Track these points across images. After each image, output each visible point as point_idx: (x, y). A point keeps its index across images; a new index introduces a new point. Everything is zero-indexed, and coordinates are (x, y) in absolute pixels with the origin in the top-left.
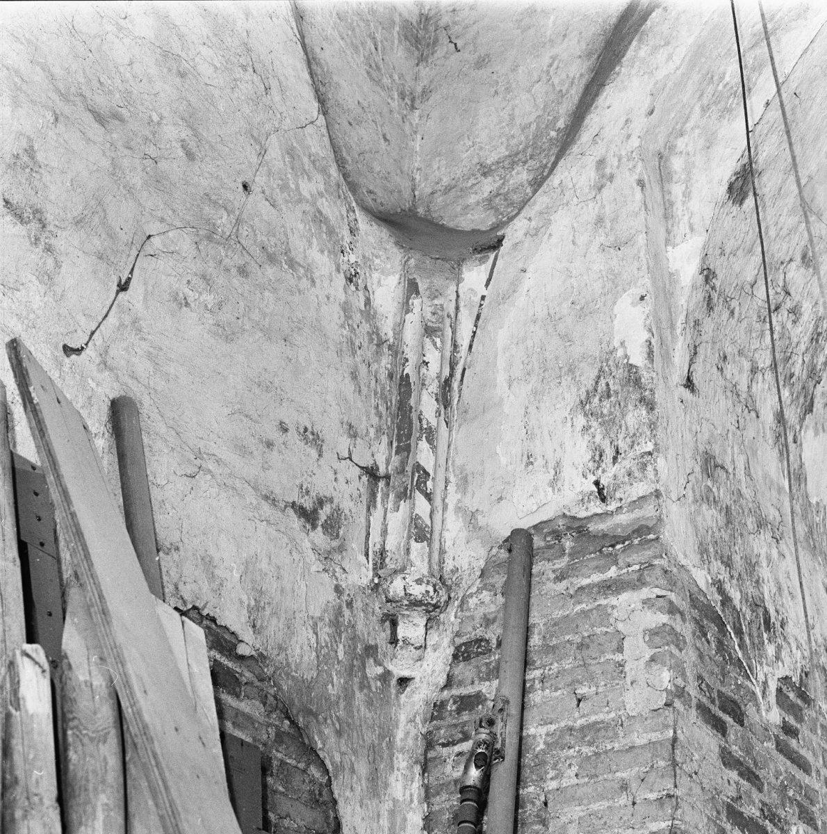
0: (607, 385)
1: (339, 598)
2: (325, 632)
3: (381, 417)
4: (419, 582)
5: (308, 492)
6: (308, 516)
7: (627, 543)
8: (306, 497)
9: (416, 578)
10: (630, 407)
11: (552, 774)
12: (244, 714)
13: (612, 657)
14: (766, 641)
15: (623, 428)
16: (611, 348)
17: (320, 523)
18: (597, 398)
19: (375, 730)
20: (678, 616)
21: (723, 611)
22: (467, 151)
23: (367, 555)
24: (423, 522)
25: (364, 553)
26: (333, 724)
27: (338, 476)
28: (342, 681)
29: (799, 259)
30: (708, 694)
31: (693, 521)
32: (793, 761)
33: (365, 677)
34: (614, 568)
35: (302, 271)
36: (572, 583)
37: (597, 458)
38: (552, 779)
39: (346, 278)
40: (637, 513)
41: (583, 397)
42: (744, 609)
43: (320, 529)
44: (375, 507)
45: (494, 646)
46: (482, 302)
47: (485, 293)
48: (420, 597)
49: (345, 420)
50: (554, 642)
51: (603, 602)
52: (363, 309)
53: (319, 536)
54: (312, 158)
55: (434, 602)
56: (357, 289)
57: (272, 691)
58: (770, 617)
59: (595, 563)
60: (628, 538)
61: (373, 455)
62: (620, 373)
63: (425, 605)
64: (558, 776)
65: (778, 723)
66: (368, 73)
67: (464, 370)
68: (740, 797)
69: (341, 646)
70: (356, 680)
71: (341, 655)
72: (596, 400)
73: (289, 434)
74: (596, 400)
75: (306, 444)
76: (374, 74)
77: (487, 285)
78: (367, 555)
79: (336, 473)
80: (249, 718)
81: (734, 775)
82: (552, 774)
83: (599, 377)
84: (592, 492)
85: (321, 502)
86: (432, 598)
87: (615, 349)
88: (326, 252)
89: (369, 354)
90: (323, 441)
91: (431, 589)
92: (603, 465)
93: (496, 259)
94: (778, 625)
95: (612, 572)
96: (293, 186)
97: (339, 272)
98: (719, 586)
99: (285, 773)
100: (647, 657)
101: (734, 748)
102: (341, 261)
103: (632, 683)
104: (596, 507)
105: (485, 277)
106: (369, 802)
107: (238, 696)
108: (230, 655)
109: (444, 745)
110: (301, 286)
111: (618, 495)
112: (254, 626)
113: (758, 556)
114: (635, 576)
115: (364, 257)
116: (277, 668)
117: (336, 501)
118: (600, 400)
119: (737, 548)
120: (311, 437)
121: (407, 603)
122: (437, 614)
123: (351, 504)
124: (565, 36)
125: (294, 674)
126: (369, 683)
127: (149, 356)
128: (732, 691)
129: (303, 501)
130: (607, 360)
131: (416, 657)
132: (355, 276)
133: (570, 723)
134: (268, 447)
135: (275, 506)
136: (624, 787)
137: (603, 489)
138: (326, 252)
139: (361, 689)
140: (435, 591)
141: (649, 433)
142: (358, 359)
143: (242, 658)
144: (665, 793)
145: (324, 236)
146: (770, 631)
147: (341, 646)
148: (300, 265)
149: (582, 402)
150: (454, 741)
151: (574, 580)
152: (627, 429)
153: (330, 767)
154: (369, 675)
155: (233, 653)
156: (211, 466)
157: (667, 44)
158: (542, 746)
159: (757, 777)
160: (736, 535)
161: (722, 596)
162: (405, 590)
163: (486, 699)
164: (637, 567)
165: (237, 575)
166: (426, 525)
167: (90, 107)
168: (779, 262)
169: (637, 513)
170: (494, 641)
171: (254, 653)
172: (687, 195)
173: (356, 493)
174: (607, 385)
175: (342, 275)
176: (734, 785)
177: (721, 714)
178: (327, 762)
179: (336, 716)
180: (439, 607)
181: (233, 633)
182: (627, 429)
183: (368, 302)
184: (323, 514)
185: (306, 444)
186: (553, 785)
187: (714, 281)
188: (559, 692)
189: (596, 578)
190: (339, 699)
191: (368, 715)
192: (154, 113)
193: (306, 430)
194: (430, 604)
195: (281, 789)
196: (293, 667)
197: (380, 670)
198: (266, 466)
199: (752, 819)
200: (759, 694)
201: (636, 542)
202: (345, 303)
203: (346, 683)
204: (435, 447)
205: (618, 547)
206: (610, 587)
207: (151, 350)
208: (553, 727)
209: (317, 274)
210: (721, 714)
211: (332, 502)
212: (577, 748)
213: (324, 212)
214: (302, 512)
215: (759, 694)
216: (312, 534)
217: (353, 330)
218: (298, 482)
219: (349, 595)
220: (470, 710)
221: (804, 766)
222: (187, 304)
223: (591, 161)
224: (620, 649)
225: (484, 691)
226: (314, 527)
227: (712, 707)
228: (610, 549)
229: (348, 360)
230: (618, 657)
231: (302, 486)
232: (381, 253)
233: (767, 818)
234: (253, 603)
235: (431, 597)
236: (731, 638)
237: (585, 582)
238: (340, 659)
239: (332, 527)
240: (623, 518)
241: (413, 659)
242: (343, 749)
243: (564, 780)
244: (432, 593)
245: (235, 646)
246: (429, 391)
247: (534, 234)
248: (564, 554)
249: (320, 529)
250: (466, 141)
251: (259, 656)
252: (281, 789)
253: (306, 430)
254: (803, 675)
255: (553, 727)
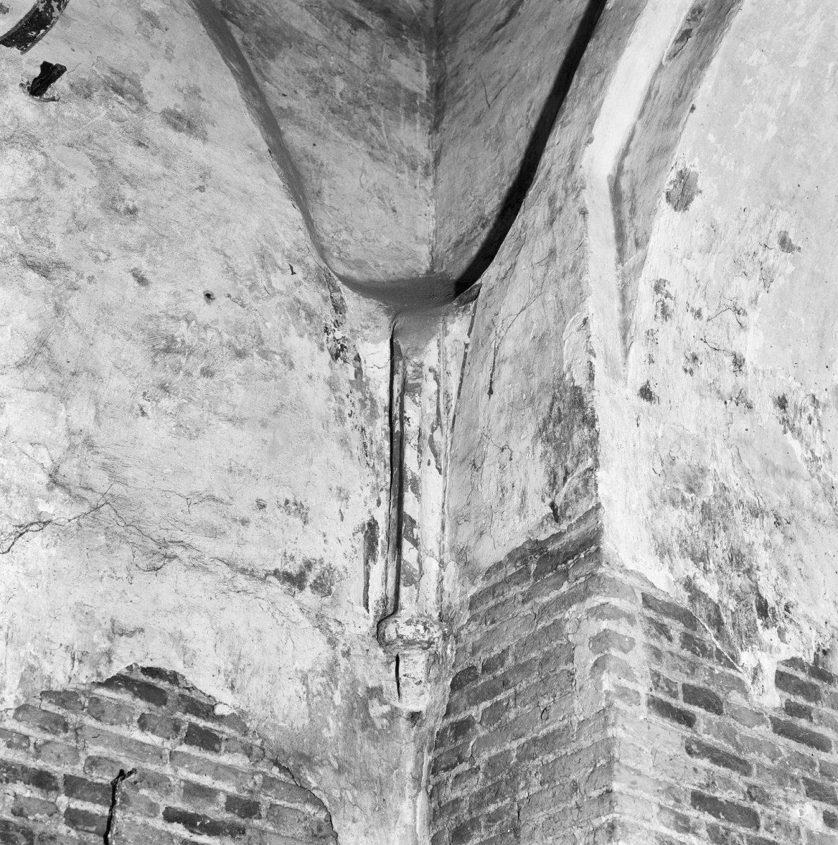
0: (559, 409)
1: (333, 648)
2: (316, 683)
4: (409, 623)
5: (292, 558)
6: (295, 581)
7: (575, 558)
8: (291, 563)
11: (522, 785)
12: (225, 767)
13: (565, 667)
15: (571, 449)
16: (562, 374)
17: (308, 584)
21: (693, 606)
23: (366, 605)
25: (362, 603)
26: (330, 764)
28: (340, 724)
36: (535, 603)
37: (552, 481)
38: (523, 789)
39: (332, 355)
40: (583, 528)
41: (541, 426)
43: (308, 589)
44: (374, 560)
45: (480, 672)
46: (466, 350)
47: (468, 341)
52: (353, 378)
54: (286, 253)
55: (426, 639)
56: (345, 362)
58: (766, 603)
59: (552, 581)
60: (577, 553)
61: (370, 512)
62: (568, 396)
63: (418, 643)
64: (527, 787)
66: (370, 154)
67: (455, 416)
70: (358, 721)
72: (551, 426)
74: (551, 426)
75: (289, 514)
77: (469, 335)
78: (366, 605)
79: (325, 536)
81: (704, 763)
82: (522, 785)
83: (552, 404)
84: (549, 514)
85: (309, 565)
86: (424, 636)
87: (564, 375)
88: (306, 336)
90: (308, 509)
91: (420, 627)
92: (557, 487)
93: (475, 307)
94: (780, 610)
97: (322, 350)
98: (689, 585)
100: (591, 662)
101: (706, 736)
103: (580, 689)
104: (552, 530)
105: (467, 326)
107: (217, 751)
110: (277, 371)
111: (568, 513)
113: (751, 545)
115: (352, 331)
118: (554, 426)
119: (717, 542)
123: (346, 562)
124: (538, 78)
125: (281, 724)
127: (104, 467)
129: (287, 567)
130: (559, 386)
132: (342, 350)
134: (243, 524)
135: (254, 576)
138: (306, 336)
139: (363, 729)
140: (425, 628)
141: (589, 450)
143: (220, 719)
144: (605, 789)
145: (304, 321)
146: (766, 616)
148: (275, 353)
149: (540, 430)
150: (452, 764)
151: (537, 600)
152: (573, 448)
153: (327, 803)
154: (372, 715)
155: (211, 714)
158: (515, 760)
159: (744, 762)
160: (717, 529)
161: (690, 591)
162: (397, 632)
163: (474, 723)
164: (583, 579)
165: (210, 643)
166: (414, 570)
167: (29, 263)
169: (583, 528)
170: (480, 667)
171: (234, 711)
172: (633, 211)
173: (350, 550)
174: (559, 409)
178: (324, 800)
179: (334, 756)
180: (433, 643)
182: (573, 448)
184: (311, 577)
185: (289, 514)
187: (666, 288)
188: (527, 707)
190: (337, 741)
195: (271, 828)
196: (280, 718)
197: (386, 709)
198: (241, 542)
200: (749, 682)
201: (582, 556)
203: (345, 725)
205: (569, 562)
207: (106, 461)
208: (523, 740)
211: (322, 563)
212: (540, 757)
213: (302, 299)
214: (287, 577)
215: (749, 682)
216: (299, 596)
218: (280, 551)
221: (821, 744)
222: (143, 414)
223: (544, 202)
225: (473, 714)
227: (673, 702)
228: (563, 565)
229: (336, 429)
230: (570, 667)
231: (285, 553)
232: (370, 324)
233: (754, 800)
236: (706, 630)
237: (546, 599)
238: (337, 704)
239: (322, 587)
240: (574, 534)
241: (416, 694)
243: (531, 788)
244: (422, 631)
245: (213, 708)
246: (412, 444)
249: (308, 589)
250: (469, 196)
252: (271, 828)
253: (287, 502)
254: (820, 654)
255: (523, 740)
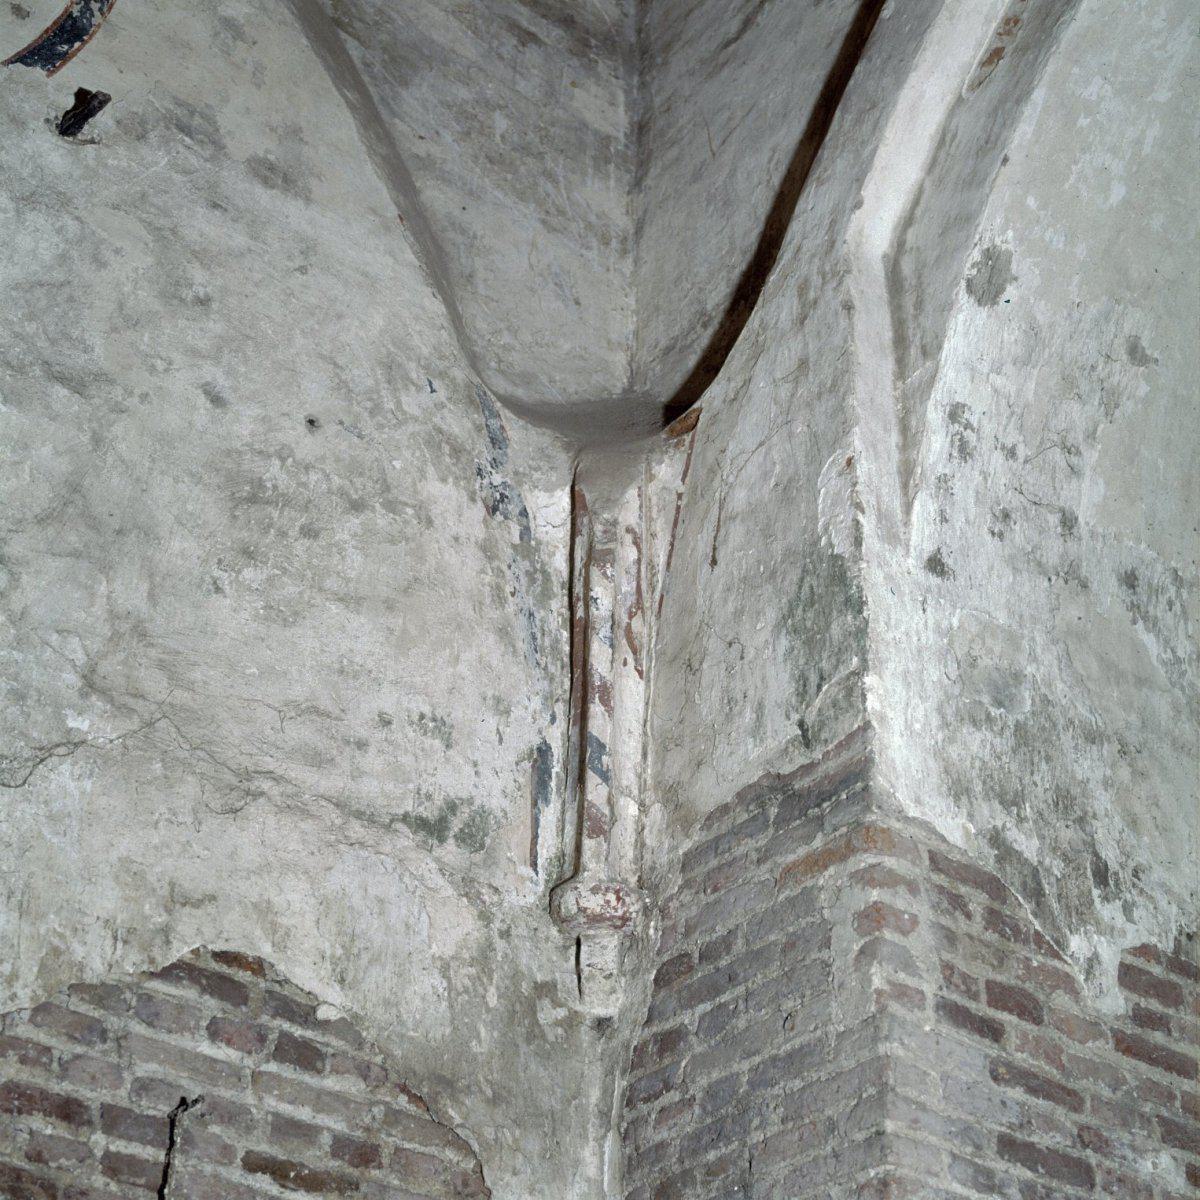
0: (811, 588)
3: (552, 680)
4: (595, 890)
5: (429, 797)
7: (834, 799)
9: (591, 886)
10: (835, 613)
11: (756, 1122)
12: (330, 1093)
13: (819, 955)
14: (1097, 901)
15: (828, 644)
16: (815, 536)
17: (452, 833)
18: (801, 607)
19: (554, 1092)
20: (902, 889)
21: (1002, 869)
22: (686, 297)
24: (598, 810)
25: (528, 863)
26: (481, 1091)
27: (480, 769)
29: (1125, 357)
30: (963, 987)
31: (938, 753)
32: (1152, 1061)
33: (535, 1023)
34: (820, 835)
35: (410, 511)
38: (756, 1129)
39: (487, 507)
40: (845, 756)
41: (785, 611)
42: (1047, 861)
43: (451, 841)
47: (682, 489)
48: (598, 910)
49: (490, 694)
50: (757, 946)
51: (809, 883)
53: (451, 852)
55: (620, 913)
56: (506, 518)
57: (379, 1059)
60: (836, 792)
64: (762, 1126)
65: (1121, 1011)
66: (544, 222)
67: (662, 597)
68: (1029, 1122)
69: (492, 990)
71: (493, 1000)
72: (800, 611)
73: (393, 727)
74: (800, 611)
76: (554, 221)
77: (683, 480)
78: (534, 865)
80: (337, 1096)
81: (1017, 1093)
82: (756, 1122)
83: (802, 580)
84: (797, 736)
86: (616, 910)
89: (530, 601)
91: (612, 897)
93: (692, 441)
94: (1126, 875)
95: (818, 842)
96: (391, 405)
98: (996, 839)
99: (403, 1161)
102: (477, 486)
105: (680, 468)
106: (546, 1187)
108: (306, 1022)
109: (646, 1100)
111: (823, 736)
112: (342, 981)
114: (843, 842)
116: (381, 1029)
117: (478, 802)
118: (804, 611)
120: (431, 725)
121: (585, 920)
122: (632, 928)
123: (506, 803)
124: (785, 115)
125: (412, 1033)
126: (542, 1031)
127: (162, 665)
128: (1018, 977)
131: (607, 988)
132: (503, 501)
133: (774, 1052)
134: (359, 748)
136: (832, 1126)
137: (807, 730)
138: (451, 480)
140: (619, 899)
142: (510, 608)
144: (874, 1130)
145: (448, 459)
146: (1106, 884)
147: (492, 990)
148: (406, 504)
151: (780, 859)
153: (476, 1147)
154: (541, 1022)
156: (266, 785)
157: (874, 106)
161: (998, 848)
163: (687, 1034)
164: (844, 830)
166: (603, 814)
168: (1088, 368)
172: (919, 305)
173: (511, 786)
174: (811, 588)
175: (480, 504)
176: (1017, 1108)
177: (992, 1013)
181: (309, 993)
182: (831, 642)
183: (526, 532)
186: (757, 1137)
189: (802, 851)
191: (542, 1073)
192: (159, 361)
193: (422, 717)
194: (614, 917)
197: (561, 1013)
199: (1056, 1152)
202: (485, 540)
203: (504, 1035)
204: (612, 709)
205: (825, 805)
206: (817, 863)
208: (757, 1059)
209: (435, 511)
210: (992, 1013)
211: (472, 804)
214: (421, 824)
216: (438, 852)
217: (499, 573)
219: (503, 921)
220: (672, 1051)
222: (218, 590)
224: (827, 944)
226: (442, 840)
227: (972, 1006)
228: (816, 810)
229: (495, 614)
231: (419, 789)
234: (339, 952)
235: (614, 908)
237: (791, 858)
238: (491, 1005)
240: (831, 766)
241: (605, 992)
242: (500, 1120)
244: (614, 902)
245: (314, 1010)
247: (733, 400)
248: (767, 826)
249: (451, 841)
251: (353, 1017)
252: (396, 1182)
253: (422, 717)
254: (1183, 939)
255: (757, 1059)
